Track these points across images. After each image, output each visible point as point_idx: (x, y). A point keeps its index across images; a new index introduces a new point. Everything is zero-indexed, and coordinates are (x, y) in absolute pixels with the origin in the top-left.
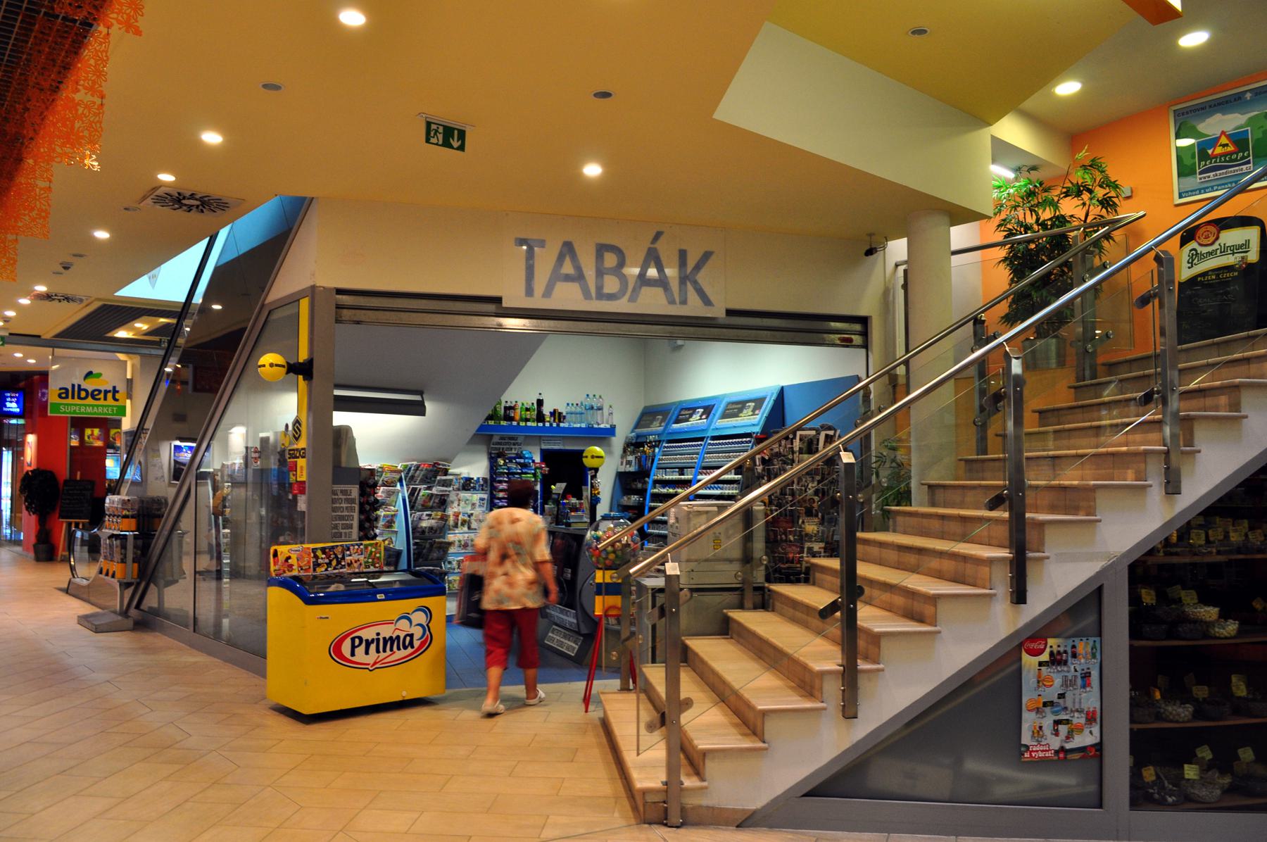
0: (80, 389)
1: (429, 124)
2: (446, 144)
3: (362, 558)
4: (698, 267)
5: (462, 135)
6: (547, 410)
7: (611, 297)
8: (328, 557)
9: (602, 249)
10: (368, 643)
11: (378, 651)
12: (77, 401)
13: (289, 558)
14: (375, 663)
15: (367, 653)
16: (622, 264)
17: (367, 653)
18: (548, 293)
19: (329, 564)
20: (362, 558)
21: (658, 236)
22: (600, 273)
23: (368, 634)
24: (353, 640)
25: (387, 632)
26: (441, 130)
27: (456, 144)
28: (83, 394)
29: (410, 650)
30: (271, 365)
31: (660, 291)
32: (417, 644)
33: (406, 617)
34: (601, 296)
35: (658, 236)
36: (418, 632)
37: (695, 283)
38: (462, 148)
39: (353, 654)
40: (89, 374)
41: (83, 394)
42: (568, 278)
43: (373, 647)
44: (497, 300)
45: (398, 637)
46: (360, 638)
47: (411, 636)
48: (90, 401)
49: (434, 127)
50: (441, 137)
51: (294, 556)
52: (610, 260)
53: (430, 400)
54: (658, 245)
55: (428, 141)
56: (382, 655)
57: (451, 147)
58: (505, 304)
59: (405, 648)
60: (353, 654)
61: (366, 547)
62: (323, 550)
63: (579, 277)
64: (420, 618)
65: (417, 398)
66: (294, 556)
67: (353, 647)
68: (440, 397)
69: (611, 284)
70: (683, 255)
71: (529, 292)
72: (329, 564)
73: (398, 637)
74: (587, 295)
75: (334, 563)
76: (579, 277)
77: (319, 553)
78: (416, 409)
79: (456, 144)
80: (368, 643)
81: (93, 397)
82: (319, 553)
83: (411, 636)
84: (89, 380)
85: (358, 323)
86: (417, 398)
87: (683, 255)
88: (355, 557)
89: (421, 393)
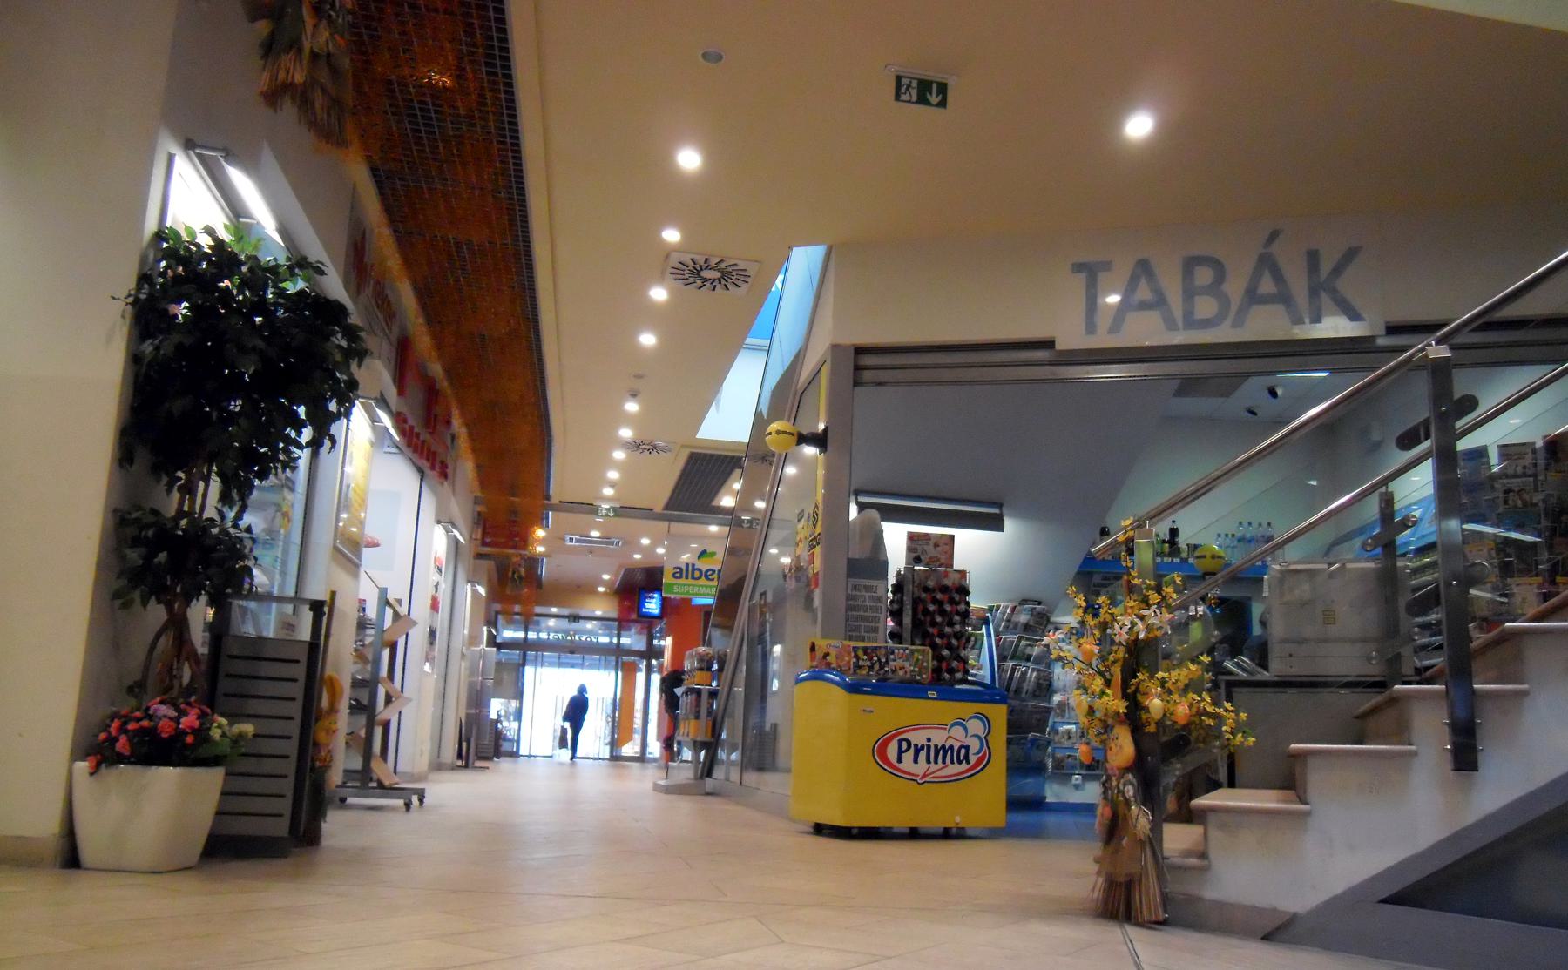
0: (694, 569)
1: (899, 79)
2: (922, 100)
3: (907, 664)
4: (1337, 271)
5: (943, 88)
6: (1182, 541)
7: (1206, 324)
8: (871, 659)
9: (1190, 264)
10: (918, 750)
11: (928, 761)
12: (690, 581)
13: (827, 654)
14: (925, 776)
15: (916, 761)
16: (1220, 277)
17: (916, 761)
18: (1115, 328)
19: (871, 668)
20: (907, 664)
21: (1274, 236)
22: (1189, 294)
23: (918, 738)
24: (900, 742)
25: (939, 738)
26: (915, 84)
27: (934, 99)
28: (697, 574)
29: (964, 766)
30: (778, 432)
31: (1279, 309)
32: (973, 759)
33: (960, 723)
34: (1191, 322)
35: (1274, 236)
36: (974, 745)
37: (1333, 292)
38: (943, 104)
39: (900, 760)
40: (703, 553)
41: (697, 574)
42: (1144, 306)
43: (923, 755)
44: (1049, 344)
45: (951, 747)
46: (909, 742)
47: (967, 748)
48: (703, 581)
49: (905, 81)
50: (914, 92)
51: (833, 653)
52: (1204, 276)
53: (1011, 516)
54: (1275, 248)
55: (897, 97)
56: (933, 767)
57: (928, 103)
58: (1058, 347)
59: (960, 762)
60: (900, 760)
61: (912, 652)
62: (865, 650)
63: (1160, 302)
64: (976, 727)
65: (995, 511)
66: (833, 653)
67: (900, 752)
68: (1024, 513)
69: (1206, 307)
70: (1313, 258)
71: (1091, 328)
72: (871, 668)
73: (951, 747)
74: (1170, 324)
75: (877, 667)
76: (1160, 302)
77: (860, 653)
78: (995, 523)
79: (934, 99)
80: (918, 750)
81: (707, 577)
82: (860, 653)
83: (967, 748)
84: (704, 559)
85: (880, 384)
86: (995, 511)
87: (1313, 258)
88: (899, 663)
89: (1000, 506)
